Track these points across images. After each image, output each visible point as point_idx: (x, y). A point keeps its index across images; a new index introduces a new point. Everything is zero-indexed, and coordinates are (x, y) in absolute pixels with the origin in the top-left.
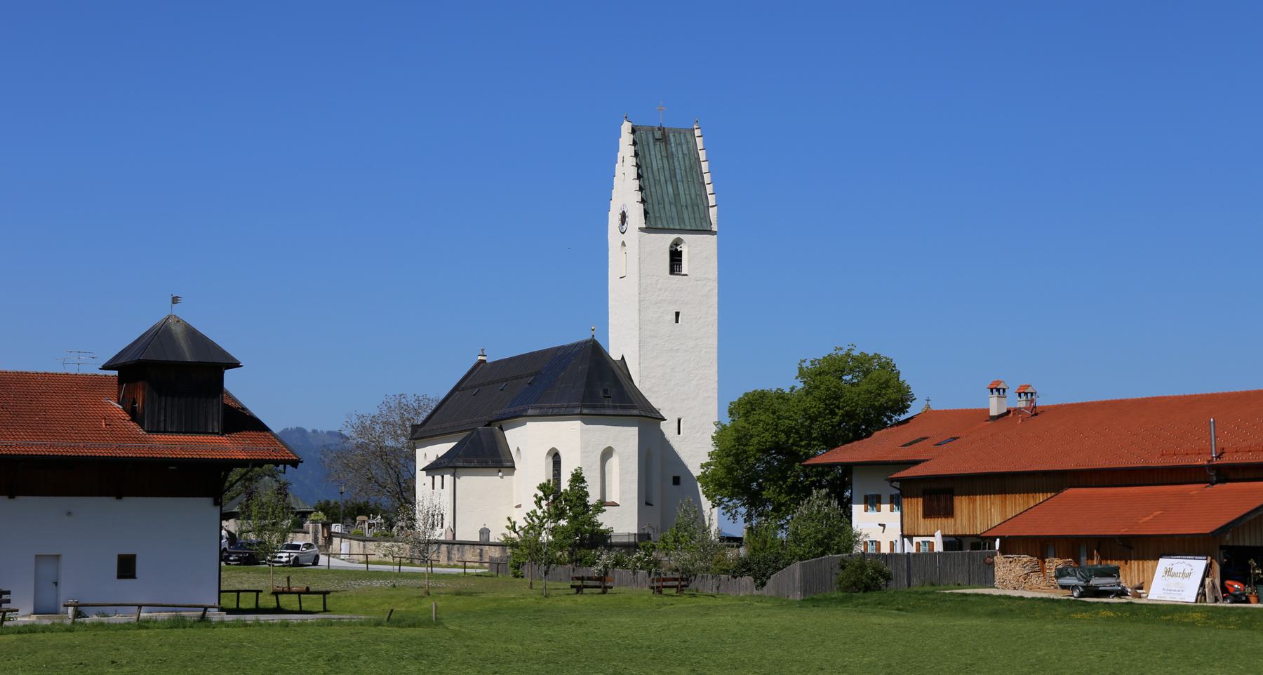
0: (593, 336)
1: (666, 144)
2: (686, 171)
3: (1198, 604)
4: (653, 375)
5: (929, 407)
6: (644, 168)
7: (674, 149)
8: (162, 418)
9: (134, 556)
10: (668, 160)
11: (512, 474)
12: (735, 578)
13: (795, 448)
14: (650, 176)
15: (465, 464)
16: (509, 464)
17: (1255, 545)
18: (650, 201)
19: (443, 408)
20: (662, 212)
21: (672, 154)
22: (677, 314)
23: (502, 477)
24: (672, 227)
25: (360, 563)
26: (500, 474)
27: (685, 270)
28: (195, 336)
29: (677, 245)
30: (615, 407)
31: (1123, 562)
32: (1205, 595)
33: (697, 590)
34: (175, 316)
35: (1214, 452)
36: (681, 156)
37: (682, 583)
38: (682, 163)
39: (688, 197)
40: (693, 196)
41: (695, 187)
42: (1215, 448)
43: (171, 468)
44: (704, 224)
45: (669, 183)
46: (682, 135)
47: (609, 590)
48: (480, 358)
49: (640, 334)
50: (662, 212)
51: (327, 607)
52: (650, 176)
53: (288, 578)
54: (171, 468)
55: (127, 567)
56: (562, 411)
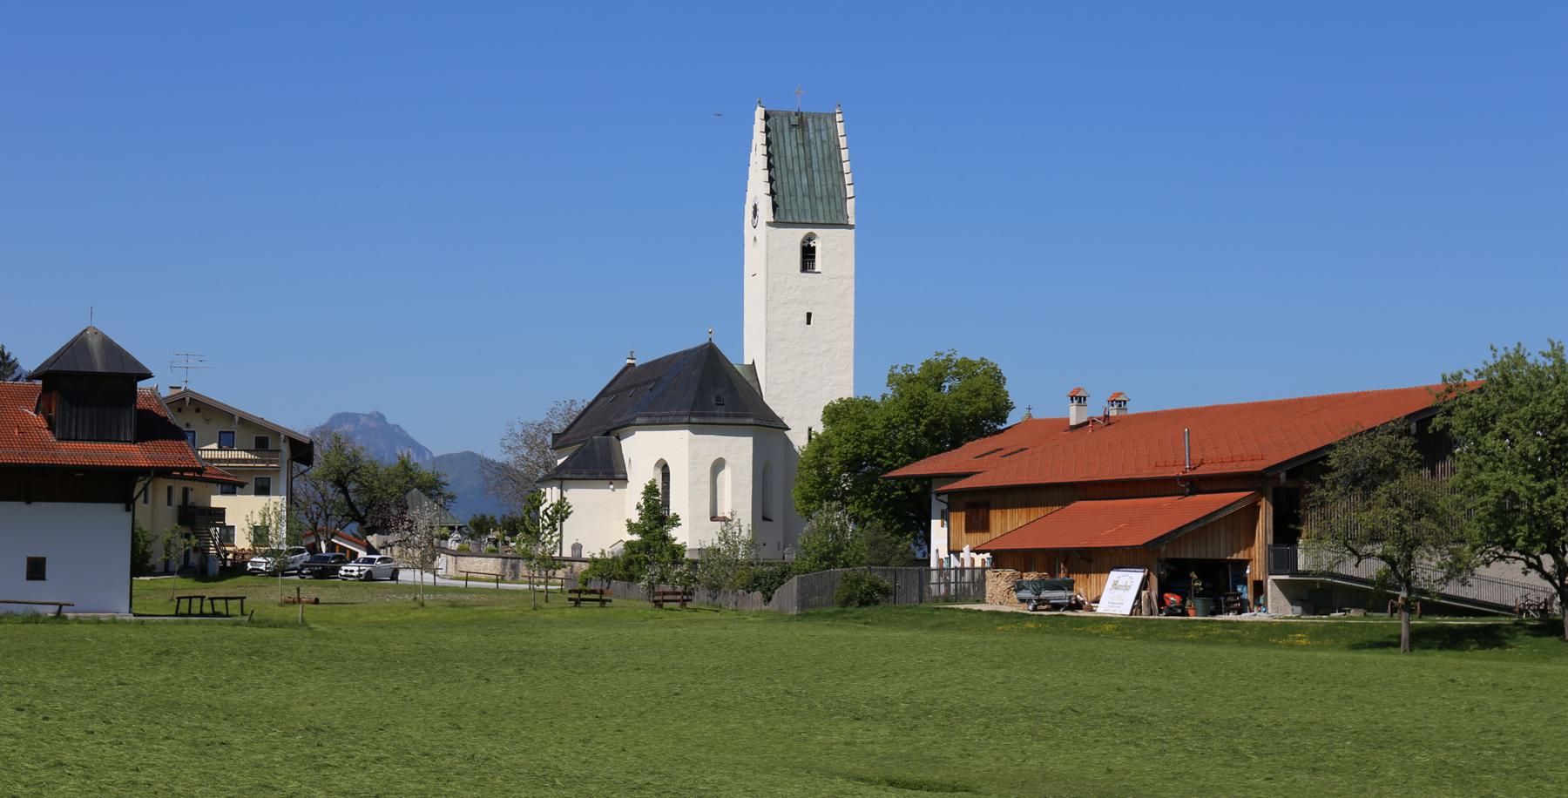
0: (710, 339)
2: (824, 160)
3: (1133, 617)
4: (781, 381)
5: (1030, 416)
6: (776, 157)
7: (811, 136)
8: (74, 427)
9: (44, 559)
11: (625, 487)
12: (749, 592)
13: (879, 459)
14: (783, 165)
15: (574, 476)
16: (621, 476)
17: (1198, 557)
18: (780, 193)
19: (587, 415)
20: (794, 203)
21: (810, 142)
22: (809, 315)
23: (613, 490)
24: (803, 221)
25: (451, 579)
26: (612, 487)
28: (110, 348)
29: (810, 240)
30: (728, 416)
31: (1085, 575)
32: (1141, 607)
33: (720, 606)
34: (94, 328)
35: (1187, 463)
36: (819, 142)
37: (685, 597)
38: (820, 151)
39: (824, 188)
40: (830, 186)
42: (1189, 458)
43: (175, 473)
44: (840, 217)
46: (822, 121)
47: (608, 604)
48: (629, 361)
49: (766, 337)
50: (794, 203)
51: (244, 612)
52: (783, 165)
53: (298, 589)
54: (175, 473)
55: (36, 569)
56: (671, 419)
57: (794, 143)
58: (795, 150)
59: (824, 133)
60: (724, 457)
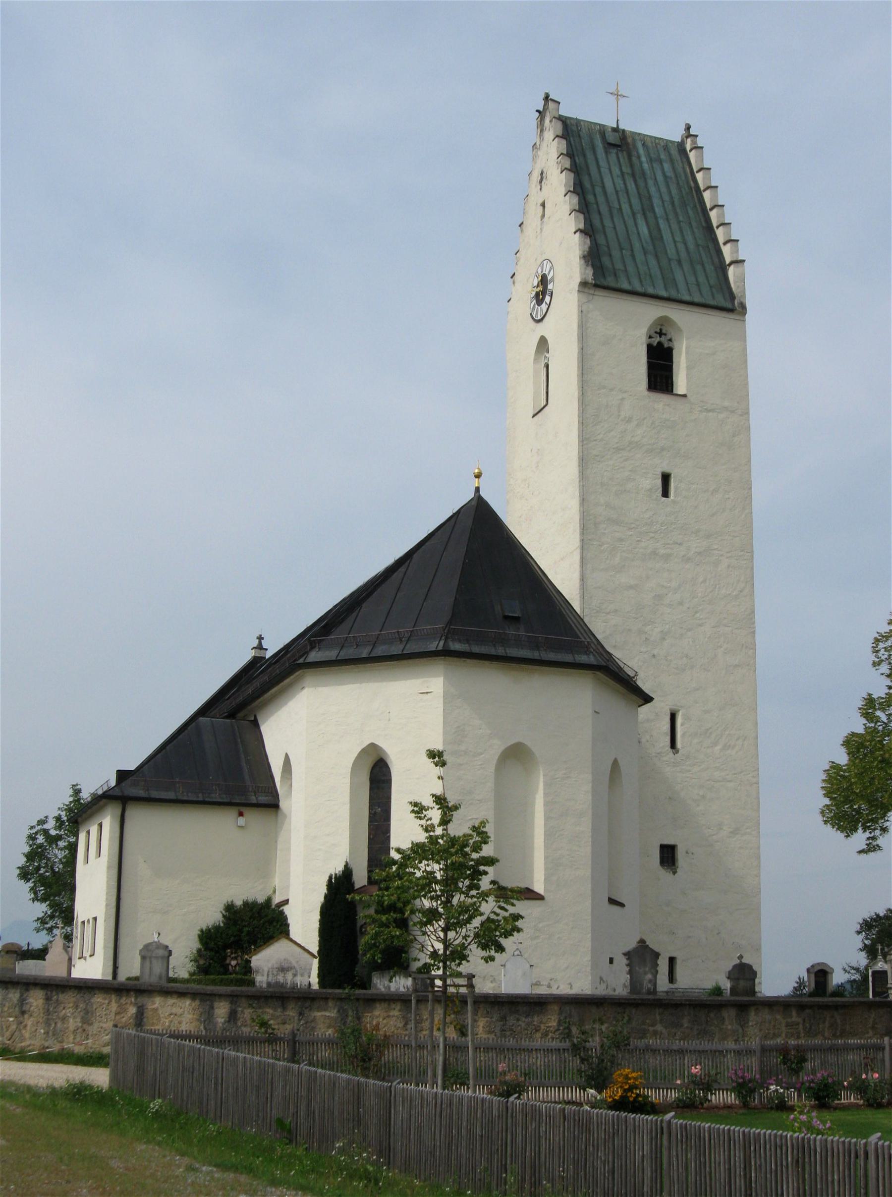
0: (477, 489)
1: (630, 156)
10: (635, 181)
20: (629, 261)
21: (643, 173)
22: (666, 478)
24: (651, 291)
27: (681, 383)
36: (660, 178)
39: (681, 246)
40: (691, 246)
41: (693, 233)
45: (639, 217)
50: (629, 261)
57: (616, 171)
58: (619, 182)
59: (667, 166)
60: (528, 743)
